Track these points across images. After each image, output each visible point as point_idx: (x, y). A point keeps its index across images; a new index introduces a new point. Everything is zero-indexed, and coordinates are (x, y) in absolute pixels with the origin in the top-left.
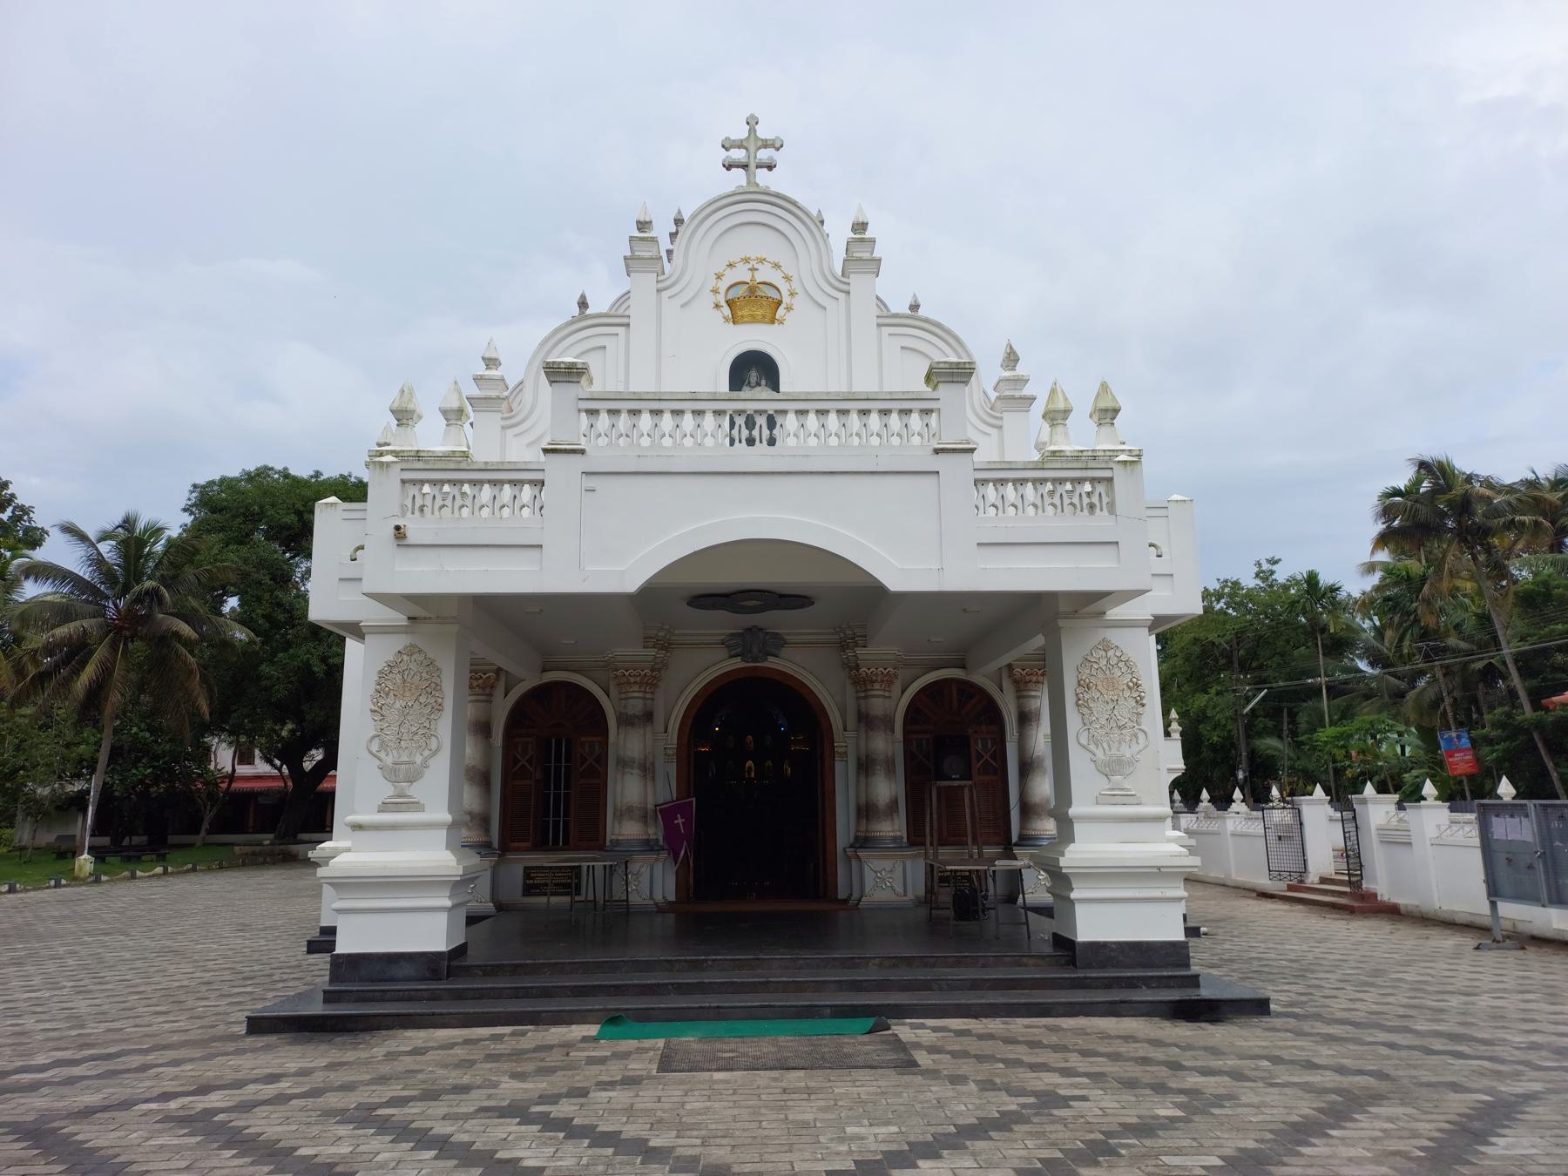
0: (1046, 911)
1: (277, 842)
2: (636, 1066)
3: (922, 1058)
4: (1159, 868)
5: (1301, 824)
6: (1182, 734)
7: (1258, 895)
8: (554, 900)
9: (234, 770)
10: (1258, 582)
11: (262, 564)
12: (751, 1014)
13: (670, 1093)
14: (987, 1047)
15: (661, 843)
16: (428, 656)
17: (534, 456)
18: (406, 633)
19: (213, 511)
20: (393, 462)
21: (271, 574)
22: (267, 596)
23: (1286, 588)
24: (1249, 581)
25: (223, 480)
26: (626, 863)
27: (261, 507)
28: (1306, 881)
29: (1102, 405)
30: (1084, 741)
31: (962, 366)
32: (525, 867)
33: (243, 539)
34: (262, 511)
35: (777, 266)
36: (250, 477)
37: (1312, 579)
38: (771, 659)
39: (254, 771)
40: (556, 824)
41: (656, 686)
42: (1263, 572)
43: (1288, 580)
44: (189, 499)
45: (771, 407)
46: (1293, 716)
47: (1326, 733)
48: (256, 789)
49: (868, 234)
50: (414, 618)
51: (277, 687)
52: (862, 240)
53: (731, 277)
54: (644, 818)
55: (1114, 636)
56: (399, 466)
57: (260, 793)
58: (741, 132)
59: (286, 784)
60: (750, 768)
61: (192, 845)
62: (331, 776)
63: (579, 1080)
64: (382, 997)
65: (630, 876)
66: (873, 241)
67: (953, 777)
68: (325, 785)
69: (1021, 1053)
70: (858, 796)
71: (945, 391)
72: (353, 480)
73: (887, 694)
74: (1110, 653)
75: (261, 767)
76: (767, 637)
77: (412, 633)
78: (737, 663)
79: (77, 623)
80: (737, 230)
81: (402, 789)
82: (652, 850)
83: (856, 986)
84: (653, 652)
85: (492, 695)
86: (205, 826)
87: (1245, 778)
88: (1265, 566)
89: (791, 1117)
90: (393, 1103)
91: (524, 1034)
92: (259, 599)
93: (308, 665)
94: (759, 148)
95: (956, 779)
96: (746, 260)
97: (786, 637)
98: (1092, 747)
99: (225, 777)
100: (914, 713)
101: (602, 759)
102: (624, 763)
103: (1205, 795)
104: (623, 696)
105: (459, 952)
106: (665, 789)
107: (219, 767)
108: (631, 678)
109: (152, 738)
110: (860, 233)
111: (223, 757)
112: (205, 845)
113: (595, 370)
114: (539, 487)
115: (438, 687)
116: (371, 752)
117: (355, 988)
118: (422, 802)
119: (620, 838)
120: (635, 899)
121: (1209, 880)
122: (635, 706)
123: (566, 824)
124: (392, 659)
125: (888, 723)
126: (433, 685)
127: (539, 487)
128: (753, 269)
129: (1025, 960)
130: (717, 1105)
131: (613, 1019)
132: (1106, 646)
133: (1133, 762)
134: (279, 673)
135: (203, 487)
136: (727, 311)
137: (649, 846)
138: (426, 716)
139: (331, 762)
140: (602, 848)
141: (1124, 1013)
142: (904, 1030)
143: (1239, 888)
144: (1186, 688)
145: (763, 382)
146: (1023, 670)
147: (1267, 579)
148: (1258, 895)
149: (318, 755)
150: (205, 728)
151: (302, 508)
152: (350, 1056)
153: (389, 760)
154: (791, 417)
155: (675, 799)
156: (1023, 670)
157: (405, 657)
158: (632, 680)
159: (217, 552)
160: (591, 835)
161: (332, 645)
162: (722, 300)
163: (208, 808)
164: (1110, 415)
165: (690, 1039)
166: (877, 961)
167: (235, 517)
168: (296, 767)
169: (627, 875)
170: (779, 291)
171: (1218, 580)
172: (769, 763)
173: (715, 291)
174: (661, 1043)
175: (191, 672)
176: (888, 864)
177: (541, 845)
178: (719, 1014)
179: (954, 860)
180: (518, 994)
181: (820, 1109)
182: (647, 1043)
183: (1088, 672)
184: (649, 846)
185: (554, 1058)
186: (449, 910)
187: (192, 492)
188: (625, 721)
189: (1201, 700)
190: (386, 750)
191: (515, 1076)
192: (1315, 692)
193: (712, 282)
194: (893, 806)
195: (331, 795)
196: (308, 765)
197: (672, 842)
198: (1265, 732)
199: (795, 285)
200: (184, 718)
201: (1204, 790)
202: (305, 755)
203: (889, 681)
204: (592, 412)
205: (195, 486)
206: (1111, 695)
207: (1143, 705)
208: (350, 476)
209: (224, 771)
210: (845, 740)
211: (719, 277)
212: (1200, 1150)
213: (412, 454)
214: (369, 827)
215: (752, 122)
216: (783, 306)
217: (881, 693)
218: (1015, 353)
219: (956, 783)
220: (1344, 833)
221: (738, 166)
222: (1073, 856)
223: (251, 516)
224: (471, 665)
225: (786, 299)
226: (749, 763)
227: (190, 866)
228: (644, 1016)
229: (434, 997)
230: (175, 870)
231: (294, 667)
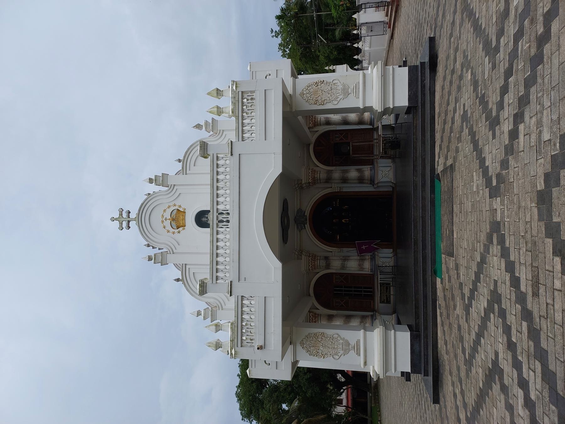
0: (397, 117)
2: (452, 265)
3: (449, 162)
4: (382, 76)
5: (367, 23)
7: (392, 39)
8: (392, 293)
9: (344, 406)
10: (279, 37)
12: (433, 223)
13: (461, 252)
14: (446, 139)
15: (371, 254)
17: (233, 299)
19: (251, 413)
20: (234, 350)
22: (282, 394)
23: (281, 27)
24: (279, 40)
25: (240, 410)
26: (378, 266)
27: (250, 396)
28: (387, 21)
29: (215, 94)
30: (336, 102)
31: (201, 145)
32: (380, 303)
33: (262, 402)
35: (165, 211)
36: (239, 400)
37: (278, 17)
38: (306, 214)
39: (345, 399)
40: (365, 291)
41: (315, 255)
43: (279, 26)
44: (247, 421)
45: (215, 214)
46: (327, 25)
47: (334, 13)
49: (154, 178)
50: (291, 342)
52: (156, 180)
53: (169, 227)
54: (362, 260)
55: (299, 91)
56: (236, 348)
58: (117, 223)
59: (350, 388)
60: (345, 221)
63: (457, 286)
64: (426, 355)
65: (383, 265)
66: (156, 176)
67: (349, 149)
68: (350, 373)
69: (448, 127)
70: (355, 183)
71: (210, 152)
72: (240, 363)
73: (319, 172)
74: (305, 93)
75: (344, 396)
76: (298, 215)
77: (296, 343)
78: (307, 226)
80: (152, 225)
82: (374, 257)
83: (424, 185)
84: (303, 257)
85: (318, 314)
86: (364, 416)
87: (350, 42)
88: (274, 34)
89: (470, 210)
90: (464, 353)
91: (440, 305)
92: (283, 397)
94: (122, 217)
95: (350, 148)
96: (163, 222)
97: (298, 208)
98: (338, 99)
99: (347, 409)
101: (341, 275)
102: (343, 267)
103: (356, 57)
104: (319, 267)
105: (410, 328)
106: (352, 252)
110: (153, 181)
111: (340, 410)
114: (244, 298)
115: (315, 334)
117: (423, 365)
119: (370, 269)
120: (392, 264)
121: (386, 56)
122: (323, 263)
123: (365, 288)
125: (329, 172)
126: (315, 336)
127: (244, 298)
128: (166, 219)
129: (414, 125)
130: (466, 237)
131: (435, 273)
132: (302, 94)
133: (344, 85)
135: (243, 416)
136: (181, 229)
137: (373, 258)
140: (373, 275)
141: (434, 89)
142: (440, 169)
143: (389, 45)
144: (317, 63)
145: (206, 216)
146: (311, 123)
147: (278, 33)
148: (392, 39)
149: (339, 376)
150: (329, 416)
152: (447, 368)
153: (342, 352)
154: (219, 207)
155: (356, 249)
156: (311, 123)
157: (305, 346)
158: (313, 264)
160: (369, 279)
162: (176, 231)
163: (358, 415)
164: (219, 92)
165: (442, 245)
166: (414, 177)
167: (254, 406)
168: (343, 384)
169: (383, 266)
170: (174, 210)
171: (278, 51)
172: (343, 214)
173: (174, 233)
174: (443, 256)
175: (309, 421)
176: (380, 172)
177: (372, 297)
178: (433, 235)
179: (379, 149)
180: (425, 306)
181: (467, 200)
182: (443, 261)
183: (311, 101)
184: (373, 258)
185: (449, 295)
186: (395, 331)
187: (245, 421)
188: (328, 266)
189: (322, 58)
191: (455, 309)
192: (319, 17)
193: (170, 234)
194: (359, 171)
195: (354, 373)
196: (343, 380)
197: (371, 250)
198: (333, 35)
201: (354, 57)
202: (339, 381)
203: (314, 172)
204: (217, 278)
205: (242, 419)
206: (320, 92)
207: (323, 81)
209: (345, 410)
210: (335, 187)
211: (168, 231)
212: (483, 64)
213: (232, 343)
215: (113, 219)
216: (179, 208)
217: (318, 174)
218: (196, 125)
219: (351, 148)
220: (370, 8)
221: (129, 224)
222: (377, 106)
224: (307, 322)
225: (177, 207)
226: (343, 221)
228: (434, 262)
229: (426, 337)
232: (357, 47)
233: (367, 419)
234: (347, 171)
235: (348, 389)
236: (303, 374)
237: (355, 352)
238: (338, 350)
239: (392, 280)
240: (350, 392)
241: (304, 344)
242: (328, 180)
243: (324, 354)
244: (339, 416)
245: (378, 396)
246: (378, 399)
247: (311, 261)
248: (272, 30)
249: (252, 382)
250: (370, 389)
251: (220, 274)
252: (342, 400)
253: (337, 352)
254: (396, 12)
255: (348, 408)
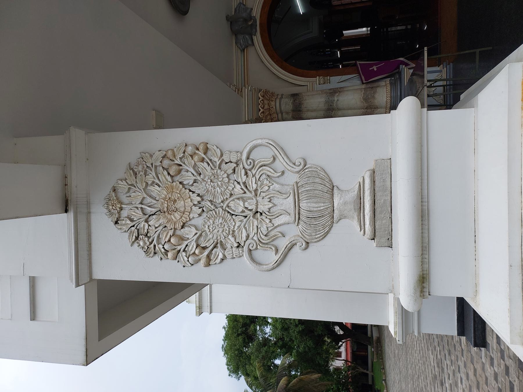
1: (372, 345)
9: (343, 360)
11: (258, 350)
16: (122, 175)
18: (89, 213)
21: (263, 346)
25: (227, 365)
27: (236, 350)
33: (249, 358)
34: (238, 350)
39: (344, 352)
48: (351, 351)
51: (308, 345)
59: (349, 340)
61: (373, 377)
62: (345, 324)
68: (349, 325)
77: (88, 204)
78: (257, 39)
81: (345, 203)
86: (365, 371)
92: (273, 352)
93: (299, 332)
99: (346, 363)
107: (342, 365)
108: (265, 108)
109: (331, 390)
111: (338, 363)
112: (372, 371)
116: (279, 264)
118: (372, 166)
124: (127, 234)
126: (166, 162)
134: (302, 344)
138: (216, 171)
139: (340, 325)
149: (337, 328)
151: (236, 334)
158: (266, 107)
159: (254, 368)
161: (291, 323)
163: (358, 370)
190: (275, 238)
195: (353, 325)
196: (342, 332)
200: (320, 384)
202: (337, 333)
205: (229, 375)
208: (227, 315)
209: (344, 363)
214: (423, 263)
223: (241, 353)
227: (383, 382)
230: (385, 389)
231: (300, 338)
233: (368, 374)
235: (347, 342)
236: (294, 326)
237: (362, 226)
238: (277, 222)
239: (448, 104)
240: (349, 345)
241: (121, 203)
243: (210, 244)
244: (337, 369)
246: (382, 354)
247: (262, 100)
249: (237, 335)
250: (372, 343)
252: (341, 353)
253: (272, 233)
255: (348, 362)
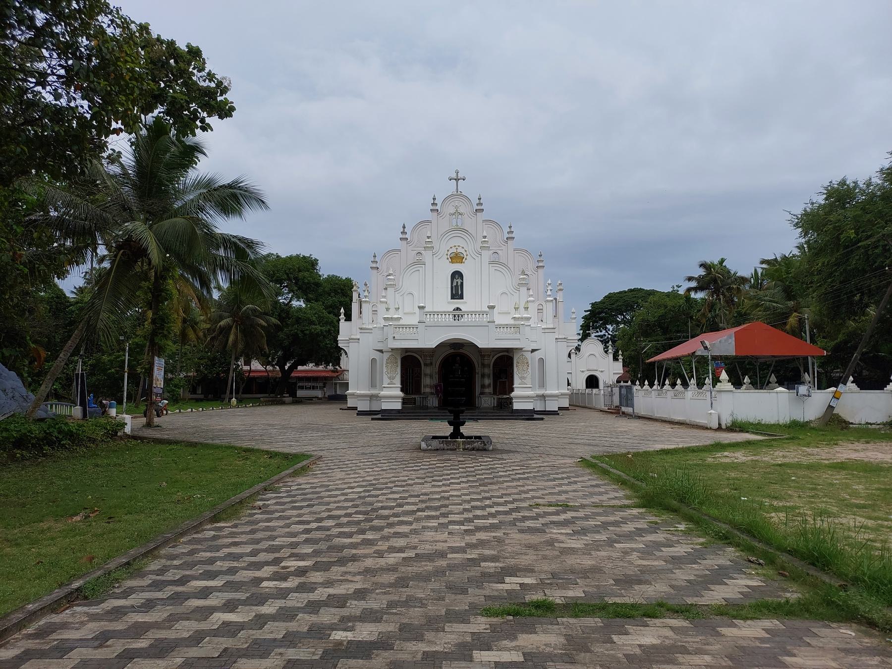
6: (623, 359)
35: (463, 248)
42: (674, 291)
54: (431, 387)
55: (524, 353)
57: (258, 378)
58: (454, 176)
72: (301, 256)
78: (452, 351)
79: (225, 320)
88: (676, 288)
96: (455, 246)
100: (495, 363)
102: (426, 375)
106: (435, 381)
113: (348, 323)
120: (429, 405)
122: (428, 362)
125: (489, 366)
136: (450, 260)
137: (432, 394)
168: (282, 368)
173: (447, 255)
176: (487, 398)
180: (414, 416)
184: (432, 394)
188: (426, 365)
194: (489, 386)
196: (286, 368)
197: (437, 393)
199: (468, 253)
210: (478, 370)
211: (448, 251)
215: (457, 173)
221: (453, 179)
225: (465, 257)
232: (706, 382)
234: (489, 376)
242: (483, 365)
245: (277, 404)
248: (680, 287)
251: (428, 316)
254: (611, 412)
